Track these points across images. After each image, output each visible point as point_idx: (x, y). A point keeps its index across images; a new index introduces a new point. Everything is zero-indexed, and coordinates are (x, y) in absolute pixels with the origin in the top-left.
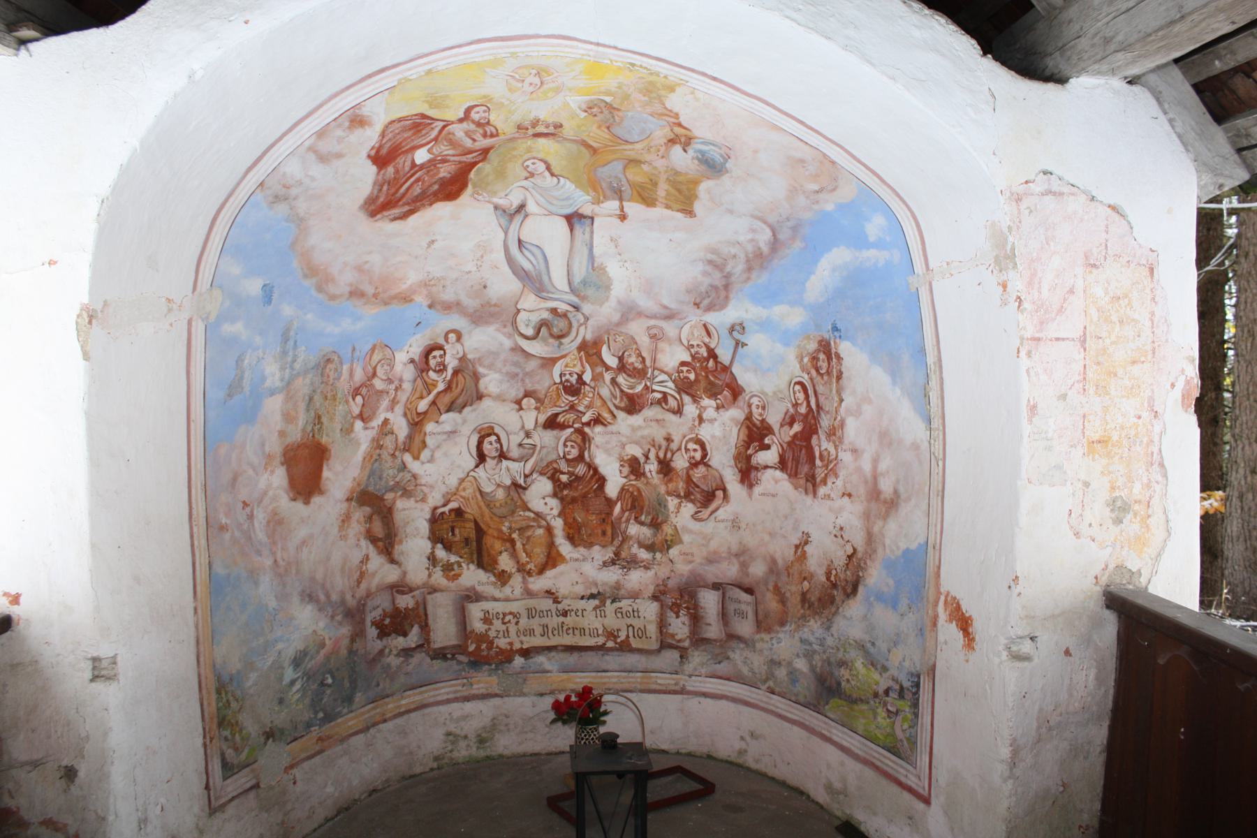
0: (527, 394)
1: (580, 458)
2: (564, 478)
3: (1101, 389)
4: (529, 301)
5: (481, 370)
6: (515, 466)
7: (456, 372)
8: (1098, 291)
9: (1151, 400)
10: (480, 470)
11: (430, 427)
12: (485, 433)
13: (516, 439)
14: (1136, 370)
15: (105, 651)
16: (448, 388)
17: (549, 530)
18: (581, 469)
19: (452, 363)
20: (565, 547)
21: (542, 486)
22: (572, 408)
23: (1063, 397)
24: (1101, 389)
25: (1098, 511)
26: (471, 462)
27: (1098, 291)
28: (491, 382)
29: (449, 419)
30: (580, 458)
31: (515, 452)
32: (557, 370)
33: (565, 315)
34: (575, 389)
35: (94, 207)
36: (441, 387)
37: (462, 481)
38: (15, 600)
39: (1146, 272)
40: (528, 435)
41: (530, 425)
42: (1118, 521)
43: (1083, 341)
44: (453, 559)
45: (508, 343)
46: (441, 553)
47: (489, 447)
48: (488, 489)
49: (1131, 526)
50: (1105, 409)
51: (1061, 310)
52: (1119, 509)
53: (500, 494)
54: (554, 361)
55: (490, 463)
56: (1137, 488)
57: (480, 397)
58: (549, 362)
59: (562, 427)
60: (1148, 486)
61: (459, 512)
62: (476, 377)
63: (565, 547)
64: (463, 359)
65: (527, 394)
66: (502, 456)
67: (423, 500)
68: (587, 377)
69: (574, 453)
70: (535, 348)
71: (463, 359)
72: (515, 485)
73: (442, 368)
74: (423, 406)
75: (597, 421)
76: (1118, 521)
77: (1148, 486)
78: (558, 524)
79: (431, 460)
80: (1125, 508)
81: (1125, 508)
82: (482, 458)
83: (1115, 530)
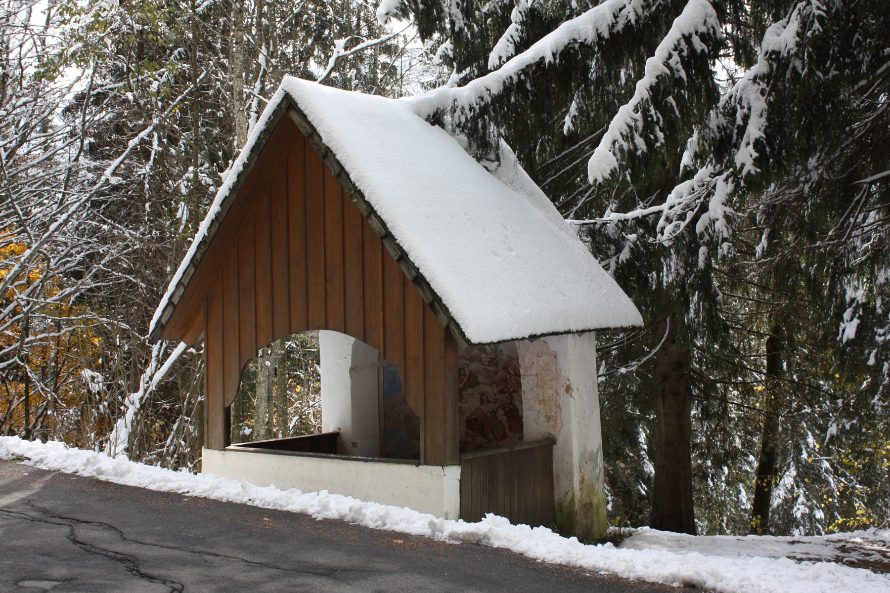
0: (493, 382)
1: (511, 403)
2: (507, 409)
3: (542, 387)
4: (483, 355)
5: (477, 375)
6: (493, 405)
7: (469, 376)
8: (541, 363)
9: (556, 390)
10: (482, 407)
11: (464, 393)
12: (482, 394)
13: (492, 396)
14: (552, 382)
15: (354, 441)
16: (468, 381)
17: (504, 426)
18: (512, 407)
19: (468, 374)
20: (508, 432)
21: (501, 412)
22: (506, 387)
23: (532, 389)
24: (542, 387)
25: (542, 419)
26: (479, 404)
27: (541, 363)
28: (481, 379)
29: (470, 390)
30: (511, 403)
31: (492, 401)
32: (499, 375)
33: (494, 359)
34: (506, 381)
35: (351, 347)
36: (466, 380)
37: (476, 409)
38: (340, 429)
39: (553, 357)
40: (495, 395)
41: (496, 392)
42: (548, 421)
43: (537, 375)
44: (474, 434)
45: (482, 367)
46: (470, 431)
47: (484, 399)
48: (485, 412)
49: (552, 423)
50: (543, 392)
51: (531, 368)
52: (548, 418)
53: (489, 414)
54: (497, 372)
55: (485, 404)
56: (553, 413)
57: (479, 383)
58: (496, 373)
59: (505, 393)
60: (556, 412)
61: (476, 419)
62: (476, 377)
63: (508, 432)
64: (470, 372)
65: (493, 382)
66: (489, 402)
67: (464, 415)
68: (508, 377)
69: (509, 402)
70: (490, 368)
71: (470, 372)
72: (493, 411)
73: (465, 375)
74: (461, 386)
75: (514, 391)
76: (548, 421)
77: (556, 412)
78: (506, 424)
79: (466, 403)
80: (550, 418)
81: (550, 418)
82: (482, 402)
83: (547, 424)
